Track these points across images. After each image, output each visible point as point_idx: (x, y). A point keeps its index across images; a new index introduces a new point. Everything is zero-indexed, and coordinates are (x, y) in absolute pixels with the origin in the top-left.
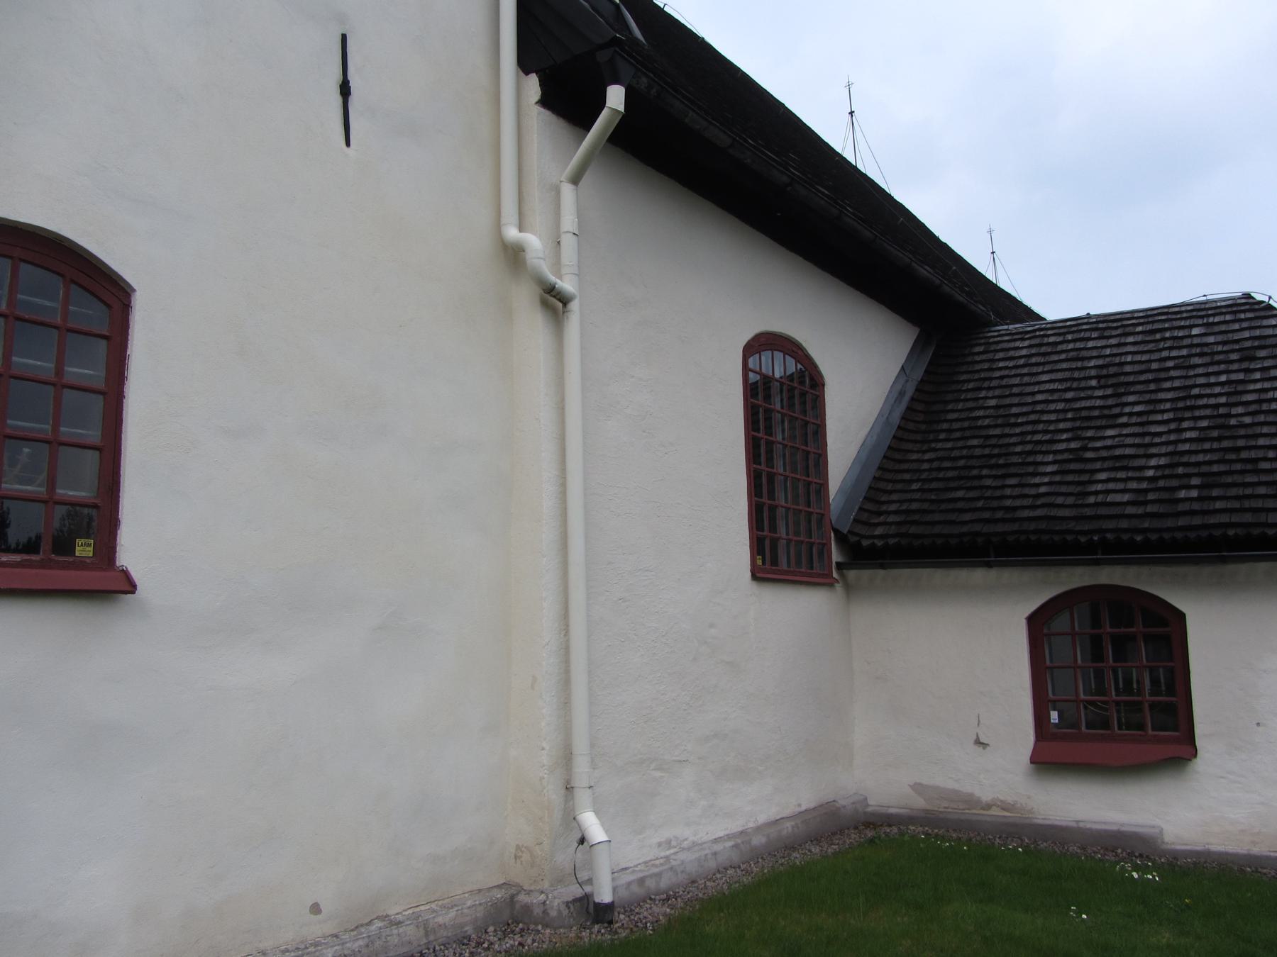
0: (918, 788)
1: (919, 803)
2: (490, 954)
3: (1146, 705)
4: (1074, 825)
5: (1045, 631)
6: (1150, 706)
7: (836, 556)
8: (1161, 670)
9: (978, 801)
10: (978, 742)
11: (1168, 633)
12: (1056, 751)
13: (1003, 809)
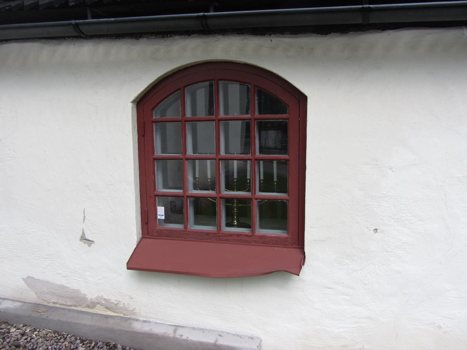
0: (30, 281)
1: (32, 297)
2: (88, 348)
3: (255, 202)
4: (170, 332)
5: (156, 116)
7: (283, 145)
8: (275, 163)
9: (84, 299)
10: (83, 238)
11: (280, 117)
13: (107, 308)
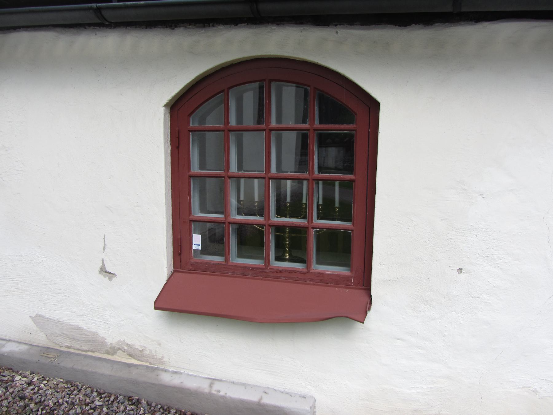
0: (39, 320)
3: (312, 232)
4: (204, 387)
6: (319, 238)
9: (103, 343)
10: (103, 271)
11: (344, 129)
12: (188, 295)
